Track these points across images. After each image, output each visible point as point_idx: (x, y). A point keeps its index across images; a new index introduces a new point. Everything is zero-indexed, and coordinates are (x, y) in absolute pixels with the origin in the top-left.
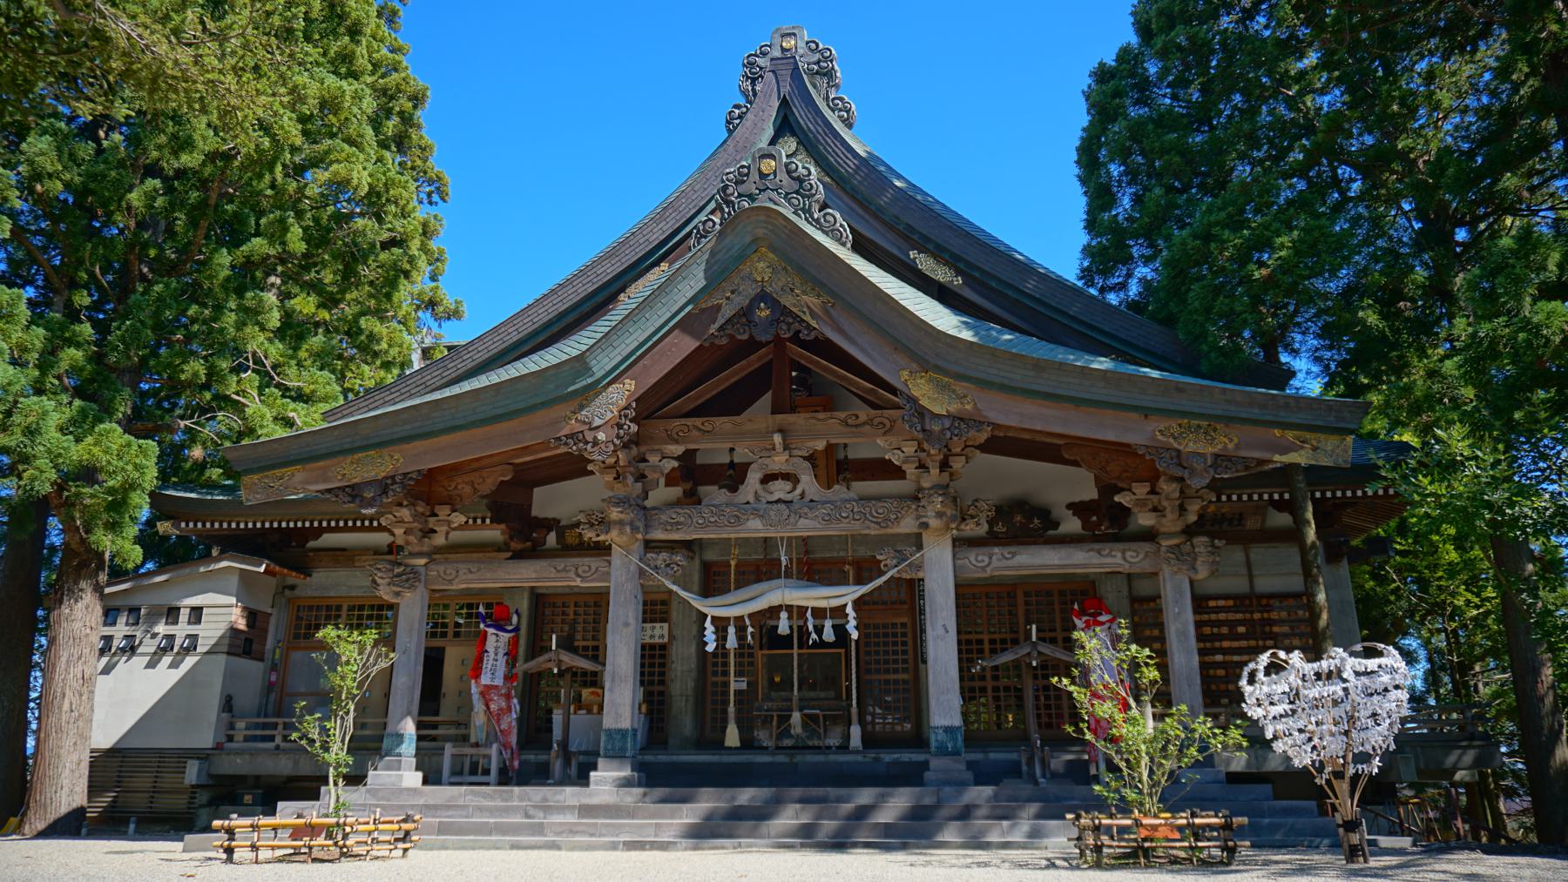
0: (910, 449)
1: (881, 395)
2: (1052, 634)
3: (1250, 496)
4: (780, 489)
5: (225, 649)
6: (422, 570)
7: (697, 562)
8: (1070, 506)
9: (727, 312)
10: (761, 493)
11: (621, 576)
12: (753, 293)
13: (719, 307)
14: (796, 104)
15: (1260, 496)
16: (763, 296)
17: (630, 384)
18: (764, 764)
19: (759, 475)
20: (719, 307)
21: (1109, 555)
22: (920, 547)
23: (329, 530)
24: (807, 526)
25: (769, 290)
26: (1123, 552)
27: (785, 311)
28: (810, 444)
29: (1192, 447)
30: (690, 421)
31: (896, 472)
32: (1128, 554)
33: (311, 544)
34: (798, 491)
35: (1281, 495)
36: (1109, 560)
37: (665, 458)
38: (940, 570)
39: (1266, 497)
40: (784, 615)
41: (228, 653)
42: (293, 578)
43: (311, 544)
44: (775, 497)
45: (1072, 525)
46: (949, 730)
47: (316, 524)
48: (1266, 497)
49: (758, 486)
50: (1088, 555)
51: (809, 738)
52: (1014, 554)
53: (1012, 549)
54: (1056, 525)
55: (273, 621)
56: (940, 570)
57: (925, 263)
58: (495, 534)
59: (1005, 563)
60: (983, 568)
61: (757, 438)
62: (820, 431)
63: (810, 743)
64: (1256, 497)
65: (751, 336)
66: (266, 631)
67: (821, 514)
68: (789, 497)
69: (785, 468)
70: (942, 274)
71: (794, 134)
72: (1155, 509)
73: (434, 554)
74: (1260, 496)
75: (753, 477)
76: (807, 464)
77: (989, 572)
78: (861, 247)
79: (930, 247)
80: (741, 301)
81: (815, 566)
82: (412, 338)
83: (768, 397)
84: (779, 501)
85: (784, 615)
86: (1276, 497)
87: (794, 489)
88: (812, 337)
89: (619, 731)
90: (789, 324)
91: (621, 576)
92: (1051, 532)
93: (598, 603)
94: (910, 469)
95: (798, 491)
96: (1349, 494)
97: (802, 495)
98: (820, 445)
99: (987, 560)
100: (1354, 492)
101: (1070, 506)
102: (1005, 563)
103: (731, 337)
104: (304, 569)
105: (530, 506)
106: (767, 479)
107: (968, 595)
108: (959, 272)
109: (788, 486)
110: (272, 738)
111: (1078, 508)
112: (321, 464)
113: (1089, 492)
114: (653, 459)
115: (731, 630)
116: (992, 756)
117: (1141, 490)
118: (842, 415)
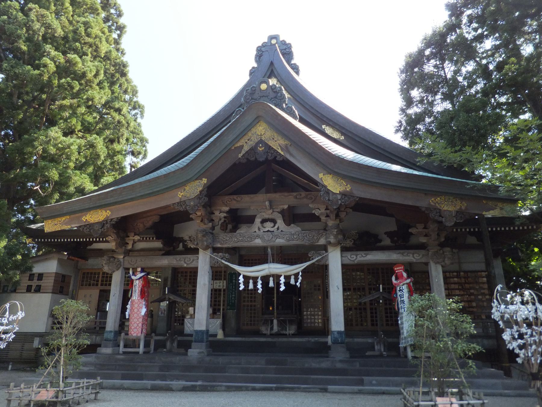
0: (323, 211)
1: (311, 186)
3: (461, 230)
4: (269, 226)
5: (51, 291)
6: (122, 260)
7: (237, 255)
8: (386, 233)
9: (246, 148)
10: (261, 227)
11: (203, 263)
12: (256, 141)
13: (242, 147)
14: (273, 59)
15: (466, 229)
16: (261, 141)
17: (205, 181)
18: (262, 342)
19: (260, 220)
20: (242, 147)
21: (407, 255)
22: (326, 251)
23: (96, 242)
24: (280, 241)
25: (263, 139)
26: (413, 254)
27: (270, 148)
28: (282, 206)
29: (446, 208)
30: (232, 197)
31: (316, 219)
32: (415, 255)
33: (89, 247)
35: (474, 229)
37: (220, 214)
38: (335, 261)
39: (468, 230)
40: (271, 279)
41: (52, 293)
42: (81, 262)
43: (89, 247)
45: (387, 241)
46: (339, 333)
47: (91, 240)
48: (468, 230)
49: (260, 225)
50: (399, 255)
51: (282, 330)
52: (366, 255)
53: (366, 252)
54: (380, 241)
55: (72, 279)
56: (335, 261)
57: (328, 130)
58: (158, 244)
59: (362, 259)
60: (353, 261)
61: (256, 203)
62: (285, 200)
63: (282, 332)
64: (463, 230)
65: (256, 159)
66: (69, 283)
67: (283, 234)
68: (272, 229)
69: (271, 217)
70: (336, 135)
71: (276, 77)
72: (426, 235)
73: (127, 253)
74: (466, 229)
75: (258, 221)
77: (356, 262)
78: (302, 121)
79: (331, 123)
80: (252, 143)
81: (285, 256)
83: (265, 188)
84: (268, 231)
85: (271, 279)
86: (472, 230)
87: (274, 226)
88: (281, 159)
89: (200, 331)
90: (272, 154)
91: (203, 263)
92: (378, 244)
93: (193, 273)
94: (323, 218)
95: (276, 227)
96: (503, 229)
97: (278, 229)
98: (286, 207)
99: (355, 257)
101: (386, 233)
103: (247, 159)
104: (86, 259)
105: (173, 232)
106: (263, 221)
107: (347, 270)
108: (343, 134)
109: (272, 225)
111: (390, 234)
112: (77, 215)
113: (393, 227)
114: (217, 213)
115: (251, 281)
116: (356, 340)
117: (420, 227)
118: (295, 194)
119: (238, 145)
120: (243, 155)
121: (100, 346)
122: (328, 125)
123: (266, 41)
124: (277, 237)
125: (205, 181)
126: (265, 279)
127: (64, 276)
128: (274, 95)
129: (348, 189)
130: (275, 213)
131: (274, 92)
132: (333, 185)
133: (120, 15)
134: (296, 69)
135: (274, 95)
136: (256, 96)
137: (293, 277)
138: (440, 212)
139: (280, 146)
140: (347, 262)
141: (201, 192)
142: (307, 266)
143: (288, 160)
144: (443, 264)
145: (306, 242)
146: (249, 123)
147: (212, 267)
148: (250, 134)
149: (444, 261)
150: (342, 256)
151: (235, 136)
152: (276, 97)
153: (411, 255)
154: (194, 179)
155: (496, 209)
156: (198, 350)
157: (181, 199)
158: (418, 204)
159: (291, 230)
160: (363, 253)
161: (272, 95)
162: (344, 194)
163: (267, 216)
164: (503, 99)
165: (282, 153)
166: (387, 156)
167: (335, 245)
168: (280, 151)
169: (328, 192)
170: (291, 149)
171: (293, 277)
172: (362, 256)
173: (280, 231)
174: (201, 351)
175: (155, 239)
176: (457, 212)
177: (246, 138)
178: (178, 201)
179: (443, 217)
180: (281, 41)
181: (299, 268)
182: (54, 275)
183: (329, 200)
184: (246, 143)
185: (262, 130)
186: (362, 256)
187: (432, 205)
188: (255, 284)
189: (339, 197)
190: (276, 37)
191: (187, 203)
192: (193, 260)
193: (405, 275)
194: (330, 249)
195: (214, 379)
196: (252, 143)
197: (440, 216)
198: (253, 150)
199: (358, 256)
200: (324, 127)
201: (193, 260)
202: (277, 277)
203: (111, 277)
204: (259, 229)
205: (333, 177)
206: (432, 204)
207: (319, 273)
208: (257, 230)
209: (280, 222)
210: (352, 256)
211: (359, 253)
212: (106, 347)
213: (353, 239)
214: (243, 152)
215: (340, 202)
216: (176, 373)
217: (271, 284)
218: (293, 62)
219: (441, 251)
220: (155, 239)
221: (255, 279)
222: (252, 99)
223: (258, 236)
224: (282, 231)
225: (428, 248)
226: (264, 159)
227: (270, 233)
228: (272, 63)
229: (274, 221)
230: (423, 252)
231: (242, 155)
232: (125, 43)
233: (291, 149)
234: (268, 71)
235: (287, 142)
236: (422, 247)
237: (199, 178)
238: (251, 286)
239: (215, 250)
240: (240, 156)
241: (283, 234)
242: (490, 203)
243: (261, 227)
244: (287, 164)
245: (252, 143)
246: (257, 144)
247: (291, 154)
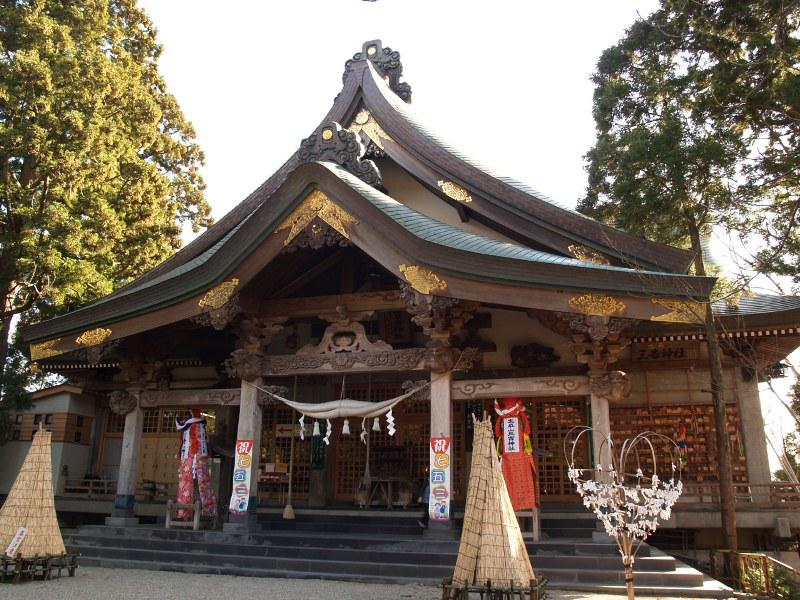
2: (102, 488)
4: (344, 342)
5: (62, 439)
9: (295, 231)
10: (332, 345)
16: (317, 220)
17: (236, 281)
19: (331, 335)
21: (554, 385)
24: (359, 367)
27: (330, 229)
34: (355, 344)
36: (554, 389)
40: (346, 422)
41: (64, 441)
44: (341, 349)
50: (541, 385)
52: (490, 385)
53: (490, 381)
59: (484, 391)
60: (470, 394)
65: (309, 246)
67: (365, 354)
68: (348, 349)
69: (347, 329)
71: (367, 109)
76: (361, 327)
77: (473, 396)
80: (302, 223)
82: (444, 285)
84: (343, 351)
85: (346, 422)
92: (555, 364)
95: (355, 344)
97: (358, 347)
99: (472, 388)
100: (756, 333)
102: (484, 391)
108: (470, 193)
109: (349, 341)
110: (86, 491)
119: (284, 226)
120: (292, 241)
121: (109, 515)
122: (446, 180)
123: (360, 51)
124: (355, 360)
125: (236, 281)
126: (337, 422)
127: (80, 419)
128: (343, 146)
129: (442, 288)
130: (355, 324)
131: (343, 141)
132: (419, 281)
133: (152, 34)
134: (404, 93)
135: (343, 146)
136: (316, 149)
137: (377, 420)
138: (584, 318)
139: (344, 226)
140: (459, 396)
141: (230, 298)
142: (398, 404)
143: (356, 246)
144: (610, 397)
145: (399, 367)
146: (297, 194)
147: (260, 405)
148: (301, 210)
149: (611, 393)
150: (451, 388)
151: (277, 215)
152: (345, 150)
153: (561, 384)
154: (221, 279)
155: (671, 311)
156: (237, 525)
157: (203, 310)
158: (550, 307)
159: (377, 349)
160: (484, 382)
161: (340, 146)
162: (436, 296)
163: (342, 329)
164: (725, 128)
165: (347, 237)
166: (540, 227)
167: (440, 372)
168: (344, 233)
169: (412, 293)
170: (360, 230)
171: (377, 420)
172: (484, 387)
173: (360, 350)
174: (241, 525)
175: (200, 363)
176: (611, 318)
177: (295, 216)
178: (199, 312)
179: (589, 327)
180: (383, 50)
181: (387, 407)
182: (65, 416)
183: (414, 305)
184: (295, 223)
185: (321, 205)
186: (484, 387)
187: (571, 308)
188: (323, 431)
189: (429, 300)
190: (374, 44)
191: (212, 314)
192: (234, 396)
193: (301, 420)
194: (433, 377)
195: (247, 564)
196: (303, 222)
197: (586, 325)
198: (304, 233)
199: (478, 387)
200: (440, 183)
201: (234, 396)
202: (355, 421)
203: (124, 420)
204: (330, 349)
205: (419, 269)
206: (572, 306)
207: (416, 413)
208: (326, 350)
209: (361, 338)
210: (468, 388)
211: (477, 382)
212: (117, 516)
213: (473, 362)
214: (291, 237)
215: (430, 308)
216: (201, 553)
217: (346, 429)
218: (401, 80)
219: (606, 378)
220: (200, 363)
221: (322, 422)
222: (311, 154)
223: (327, 360)
224: (363, 351)
225: (589, 373)
226: (320, 246)
227: (343, 354)
228: (360, 89)
229: (351, 335)
230: (579, 379)
231: (289, 241)
232: (165, 67)
233: (360, 230)
234: (354, 100)
235: (353, 219)
236: (583, 370)
237: (228, 278)
238: (316, 431)
239: (268, 381)
240: (286, 243)
241: (365, 354)
242: (662, 303)
243: (332, 345)
244: (353, 251)
245: (303, 222)
246: (312, 223)
247: (359, 238)
